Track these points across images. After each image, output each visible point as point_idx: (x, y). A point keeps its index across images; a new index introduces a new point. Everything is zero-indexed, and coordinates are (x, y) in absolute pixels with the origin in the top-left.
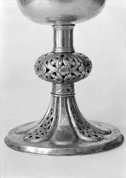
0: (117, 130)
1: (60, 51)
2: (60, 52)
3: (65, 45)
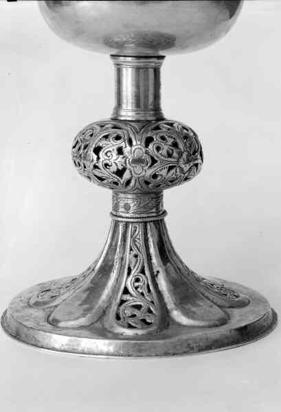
0: (261, 301)
1: (129, 116)
2: (130, 119)
3: (142, 104)
